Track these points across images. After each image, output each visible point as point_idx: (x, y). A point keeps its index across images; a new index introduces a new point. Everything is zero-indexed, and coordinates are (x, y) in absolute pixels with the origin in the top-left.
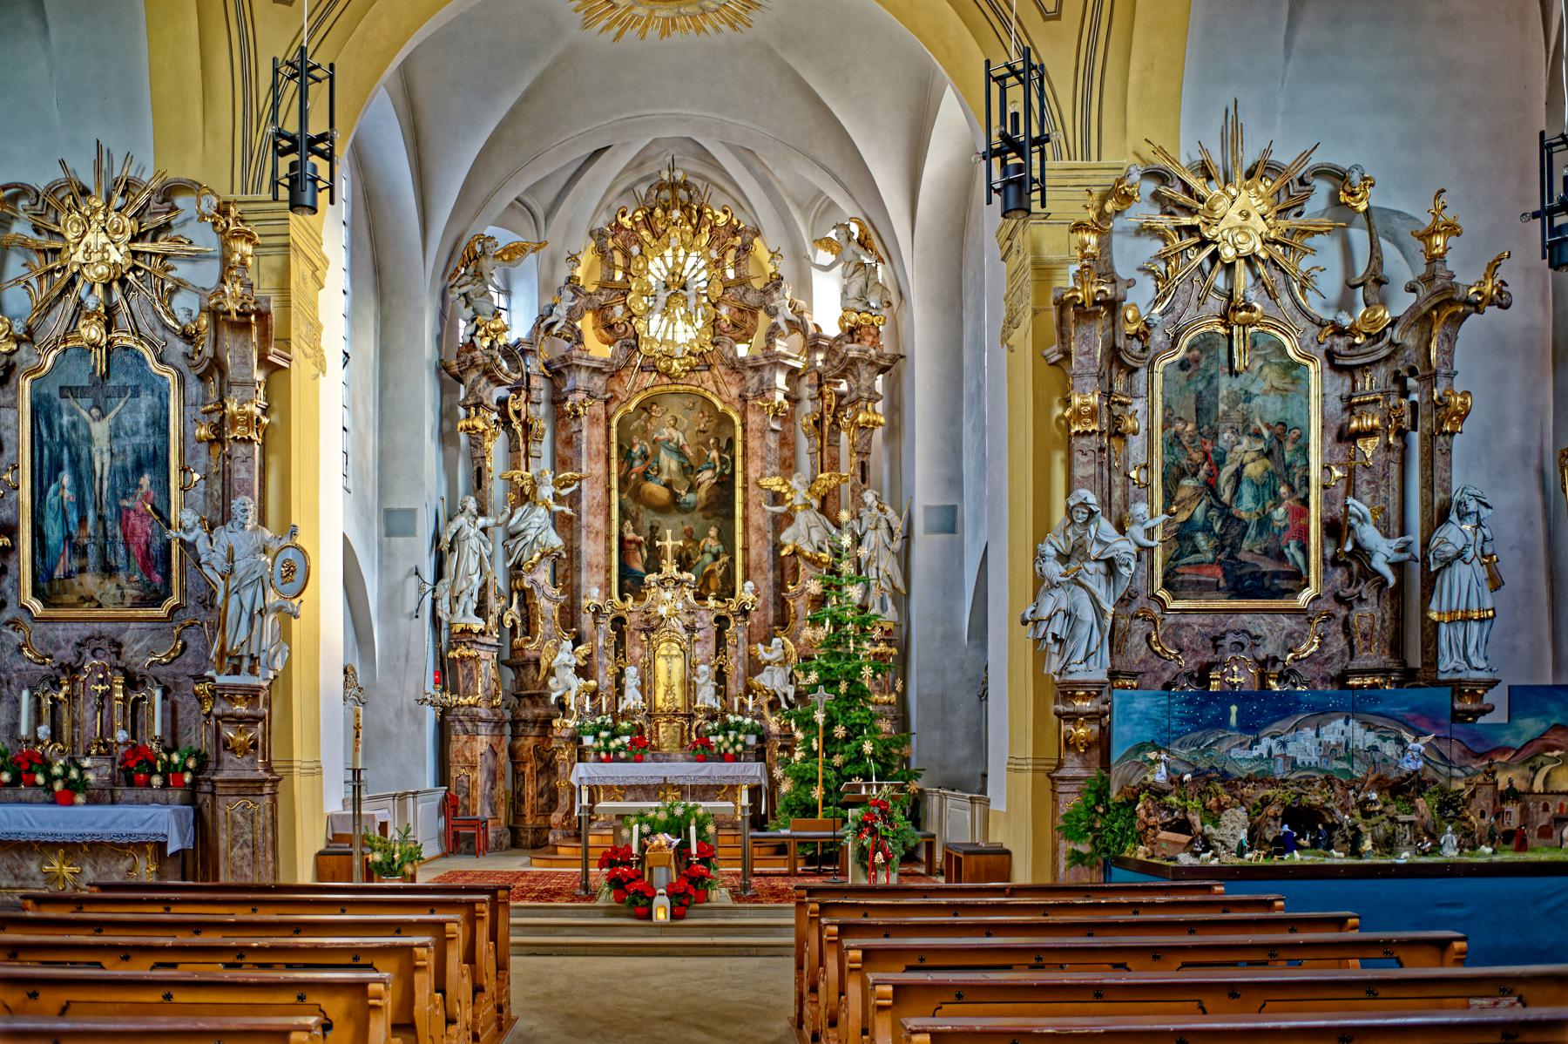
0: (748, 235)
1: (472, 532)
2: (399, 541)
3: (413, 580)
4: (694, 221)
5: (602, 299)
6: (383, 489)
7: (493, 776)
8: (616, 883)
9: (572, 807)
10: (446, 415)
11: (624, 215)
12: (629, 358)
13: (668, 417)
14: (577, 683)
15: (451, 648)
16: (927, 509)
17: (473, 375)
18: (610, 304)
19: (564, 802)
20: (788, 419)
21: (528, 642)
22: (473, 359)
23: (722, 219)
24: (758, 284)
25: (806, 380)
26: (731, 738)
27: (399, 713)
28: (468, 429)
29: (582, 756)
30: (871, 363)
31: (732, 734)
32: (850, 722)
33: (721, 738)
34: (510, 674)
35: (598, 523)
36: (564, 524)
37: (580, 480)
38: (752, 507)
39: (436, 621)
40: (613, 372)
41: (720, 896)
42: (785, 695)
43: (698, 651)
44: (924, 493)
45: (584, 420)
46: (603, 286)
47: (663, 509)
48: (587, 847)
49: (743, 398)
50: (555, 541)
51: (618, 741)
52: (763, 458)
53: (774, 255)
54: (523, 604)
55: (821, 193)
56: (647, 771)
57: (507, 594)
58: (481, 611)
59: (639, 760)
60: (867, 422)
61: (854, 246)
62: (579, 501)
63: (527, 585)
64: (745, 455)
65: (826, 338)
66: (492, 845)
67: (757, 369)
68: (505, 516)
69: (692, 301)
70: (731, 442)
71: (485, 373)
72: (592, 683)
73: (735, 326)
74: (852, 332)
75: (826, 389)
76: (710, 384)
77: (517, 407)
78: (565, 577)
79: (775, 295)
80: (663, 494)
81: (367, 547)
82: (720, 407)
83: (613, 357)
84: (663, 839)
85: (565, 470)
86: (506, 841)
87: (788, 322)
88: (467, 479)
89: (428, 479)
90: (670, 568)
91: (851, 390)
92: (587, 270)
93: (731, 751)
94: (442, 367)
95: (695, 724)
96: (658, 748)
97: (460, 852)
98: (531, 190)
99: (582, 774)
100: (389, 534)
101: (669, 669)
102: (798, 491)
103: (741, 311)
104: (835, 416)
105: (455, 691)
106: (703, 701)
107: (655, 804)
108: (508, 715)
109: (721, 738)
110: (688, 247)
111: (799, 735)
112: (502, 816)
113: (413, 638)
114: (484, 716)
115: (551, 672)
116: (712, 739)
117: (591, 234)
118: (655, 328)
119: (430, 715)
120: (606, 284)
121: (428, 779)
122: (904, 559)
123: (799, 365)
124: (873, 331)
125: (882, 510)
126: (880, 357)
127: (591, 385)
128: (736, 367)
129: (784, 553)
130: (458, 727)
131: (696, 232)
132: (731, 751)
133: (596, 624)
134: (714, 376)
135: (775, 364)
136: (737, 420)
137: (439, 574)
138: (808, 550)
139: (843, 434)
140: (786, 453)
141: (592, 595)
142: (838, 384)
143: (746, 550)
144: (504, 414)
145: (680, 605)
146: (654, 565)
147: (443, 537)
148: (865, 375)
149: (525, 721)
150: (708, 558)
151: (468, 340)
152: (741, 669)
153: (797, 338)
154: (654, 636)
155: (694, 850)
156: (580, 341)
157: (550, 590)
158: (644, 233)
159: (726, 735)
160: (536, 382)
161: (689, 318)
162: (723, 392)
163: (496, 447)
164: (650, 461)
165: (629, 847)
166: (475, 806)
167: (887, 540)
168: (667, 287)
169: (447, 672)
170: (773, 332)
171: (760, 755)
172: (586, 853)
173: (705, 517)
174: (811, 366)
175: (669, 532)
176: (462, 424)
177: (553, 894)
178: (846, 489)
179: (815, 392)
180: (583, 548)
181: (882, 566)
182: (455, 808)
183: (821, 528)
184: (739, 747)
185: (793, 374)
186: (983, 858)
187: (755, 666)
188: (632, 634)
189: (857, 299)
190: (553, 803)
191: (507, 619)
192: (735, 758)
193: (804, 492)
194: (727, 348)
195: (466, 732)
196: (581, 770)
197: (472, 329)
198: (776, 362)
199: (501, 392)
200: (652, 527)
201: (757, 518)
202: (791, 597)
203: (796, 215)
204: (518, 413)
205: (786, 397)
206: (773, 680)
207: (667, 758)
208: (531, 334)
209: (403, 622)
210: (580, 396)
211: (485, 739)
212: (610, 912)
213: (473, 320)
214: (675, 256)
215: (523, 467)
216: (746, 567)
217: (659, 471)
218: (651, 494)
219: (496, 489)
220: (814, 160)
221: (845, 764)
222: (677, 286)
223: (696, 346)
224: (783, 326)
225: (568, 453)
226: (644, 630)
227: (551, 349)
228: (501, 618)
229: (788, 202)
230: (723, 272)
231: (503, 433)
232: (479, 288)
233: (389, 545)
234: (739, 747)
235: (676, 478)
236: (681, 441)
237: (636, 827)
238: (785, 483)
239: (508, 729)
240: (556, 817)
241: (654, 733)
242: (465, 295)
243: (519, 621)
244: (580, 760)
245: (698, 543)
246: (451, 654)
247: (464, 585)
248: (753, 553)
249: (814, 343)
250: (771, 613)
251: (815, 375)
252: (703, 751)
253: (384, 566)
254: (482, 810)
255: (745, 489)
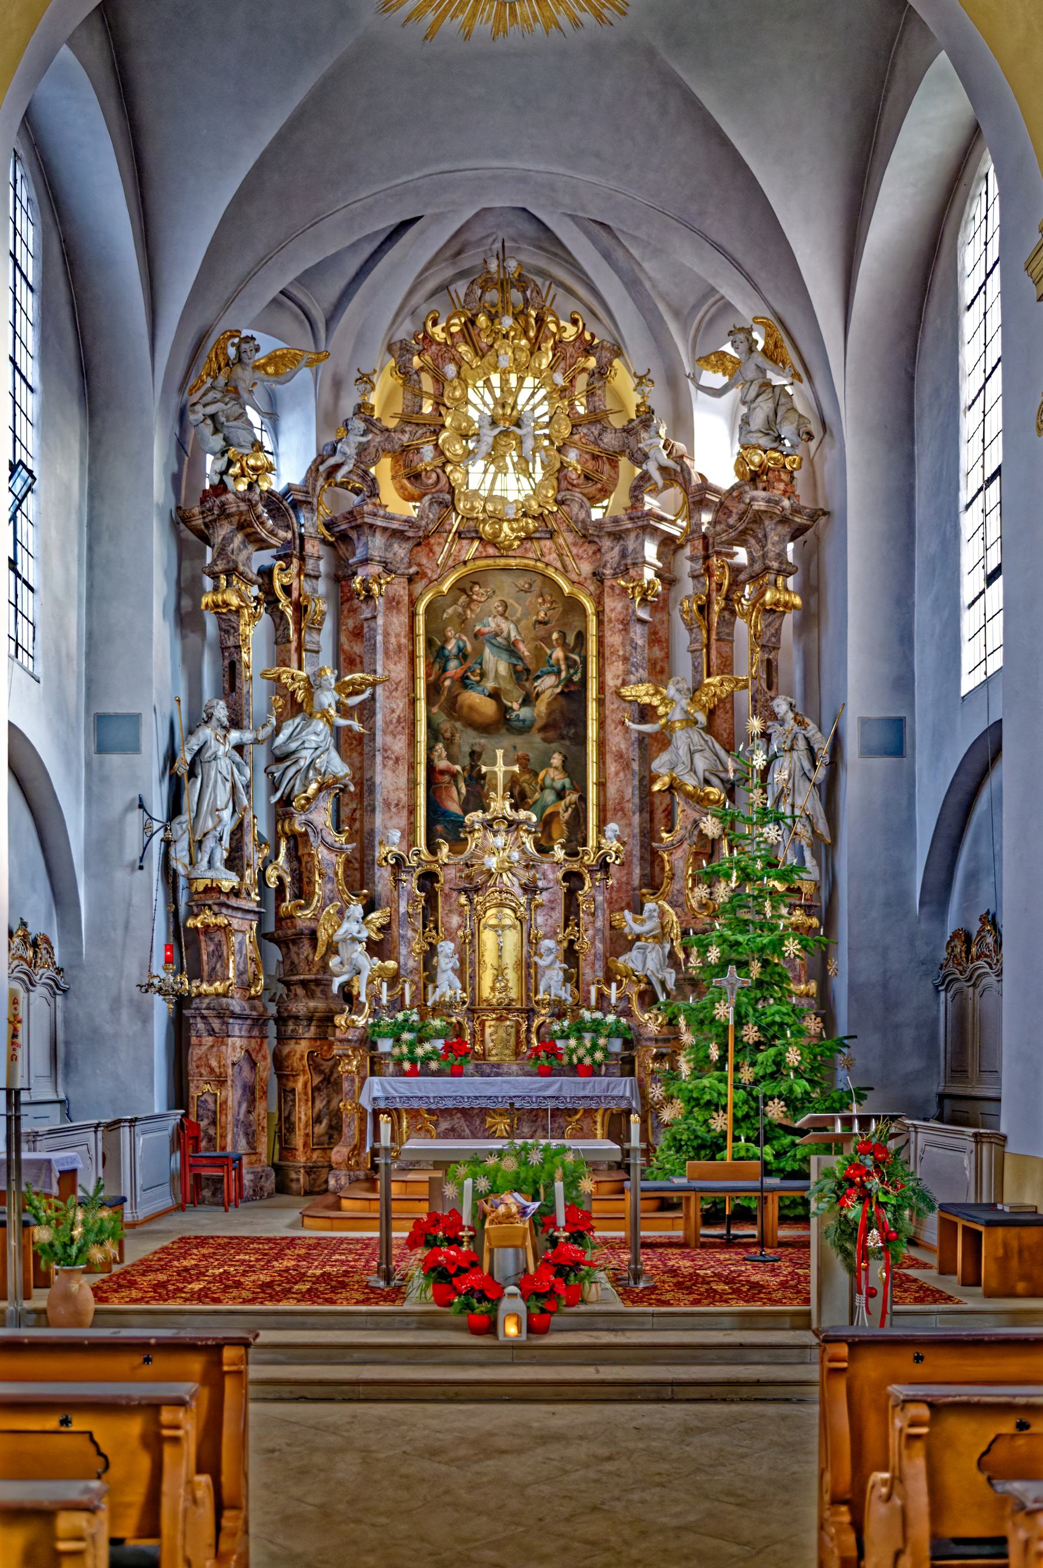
0: (606, 354)
1: (221, 750)
2: (115, 760)
3: (136, 817)
4: (532, 334)
5: (405, 438)
6: (92, 687)
7: (251, 1094)
8: (441, 1276)
9: (363, 1139)
10: (186, 588)
11: (435, 323)
12: (442, 521)
13: (495, 603)
14: (369, 964)
15: (192, 914)
16: (864, 722)
17: (223, 530)
18: (416, 446)
19: (350, 1130)
20: (660, 606)
21: (301, 907)
22: (223, 504)
23: (570, 332)
24: (617, 422)
25: (687, 551)
26: (588, 1043)
27: (115, 1005)
28: (216, 605)
29: (376, 1066)
30: (784, 520)
31: (588, 1037)
32: (765, 1021)
33: (572, 1043)
34: (275, 953)
35: (399, 745)
36: (353, 745)
37: (374, 685)
38: (610, 726)
39: (169, 874)
40: (418, 537)
41: (600, 1292)
42: (663, 983)
43: (540, 920)
44: (859, 694)
45: (380, 602)
46: (406, 420)
47: (485, 728)
48: (388, 1200)
49: (598, 576)
50: (338, 766)
51: (427, 1046)
52: (626, 659)
53: (641, 380)
54: (294, 855)
55: (713, 290)
56: (468, 1087)
57: (271, 841)
58: (234, 862)
59: (457, 1072)
60: (777, 603)
61: (759, 360)
62: (373, 714)
63: (299, 828)
64: (601, 655)
65: (716, 491)
66: (247, 1192)
67: (618, 536)
68: (269, 729)
69: (529, 444)
70: (581, 638)
71: (241, 527)
72: (391, 964)
73: (587, 478)
74: (753, 477)
75: (714, 561)
76: (552, 557)
77: (285, 580)
78: (352, 820)
79: (644, 435)
80: (488, 708)
81: (68, 764)
82: (567, 589)
83: (420, 517)
84: (512, 1201)
85: (352, 672)
86: (270, 1184)
87: (663, 469)
88: (216, 683)
89: (157, 673)
90: (500, 805)
91: (752, 559)
92: (383, 395)
93: (587, 1061)
94: (180, 518)
95: (536, 1023)
96: (484, 1056)
97: (202, 1202)
98: (307, 278)
99: (377, 1093)
100: (101, 749)
101: (499, 945)
102: (674, 703)
103: (595, 457)
104: (727, 598)
105: (195, 974)
106: (548, 990)
107: (497, 1145)
108: (272, 1009)
109: (572, 1043)
110: (522, 369)
111: (687, 1038)
112: (263, 1148)
113: (136, 900)
114: (237, 1009)
115: (332, 949)
116: (560, 1043)
117: (390, 348)
118: (477, 477)
119: (161, 1009)
120: (410, 418)
121: (158, 1101)
122: (829, 791)
123: (675, 531)
124: (783, 476)
125: (800, 723)
126: (796, 510)
127: (390, 555)
128: (589, 535)
129: (656, 788)
130: (201, 1026)
131: (535, 348)
132: (587, 1061)
133: (397, 881)
134: (558, 547)
135: (644, 528)
136: (590, 607)
137: (175, 809)
138: (690, 783)
139: (740, 623)
140: (657, 653)
141: (391, 841)
142: (733, 555)
143: (601, 785)
144: (268, 589)
145: (516, 855)
146: (477, 800)
147: (180, 755)
148: (773, 537)
149: (297, 1018)
150: (549, 796)
151: (216, 479)
152: (600, 946)
153: (675, 493)
154: (477, 899)
155: (561, 1221)
156: (374, 494)
157: (331, 836)
158: (463, 348)
159: (580, 1039)
160: (312, 548)
161: (523, 468)
162: (571, 569)
163: (255, 634)
164: (469, 663)
165: (456, 1214)
166: (223, 1136)
167: (807, 765)
168: (494, 423)
169: (186, 945)
170: (640, 486)
171: (628, 1066)
172: (388, 1211)
173: (545, 740)
174: (692, 532)
175: (500, 753)
176: (207, 599)
177: (334, 1285)
178: (744, 698)
179: (699, 567)
180: (378, 779)
181: (799, 802)
182: (197, 1140)
183: (708, 753)
184: (599, 1056)
185: (669, 545)
186: (1014, 1231)
187: (619, 942)
188: (447, 896)
189: (761, 428)
190: (335, 1129)
191: (272, 874)
192: (592, 1071)
193: (684, 702)
194: (575, 508)
195: (212, 1032)
196: (376, 1087)
197: (222, 463)
198: (645, 524)
199: (264, 558)
200: (472, 754)
201: (617, 741)
202: (666, 849)
203: (673, 327)
204: (287, 589)
205: (658, 575)
206: (646, 961)
207: (496, 1070)
208: (306, 480)
209: (121, 876)
210: (375, 569)
211: (238, 1042)
212: (426, 1322)
213: (223, 453)
214: (505, 382)
215: (294, 663)
216: (602, 809)
217: (483, 675)
218: (471, 708)
219: (257, 695)
220: (706, 238)
221: (756, 1082)
222: (508, 424)
223: (534, 505)
224: (656, 476)
225: (357, 649)
226: (465, 891)
227: (335, 500)
228: (262, 873)
229: (662, 307)
230: (571, 405)
231: (266, 617)
232: (233, 408)
233: (101, 764)
234: (599, 1056)
235: (507, 685)
236: (513, 634)
237: (468, 1182)
238: (657, 692)
239: (272, 1029)
240: (339, 1153)
241: (478, 1035)
242: (213, 417)
243: (288, 879)
244: (373, 1073)
245: (537, 775)
246: (190, 923)
247: (210, 824)
248: (612, 790)
249: (699, 496)
250: (637, 871)
251: (699, 544)
252: (548, 1060)
253: (93, 799)
254: (234, 1143)
255: (601, 702)
